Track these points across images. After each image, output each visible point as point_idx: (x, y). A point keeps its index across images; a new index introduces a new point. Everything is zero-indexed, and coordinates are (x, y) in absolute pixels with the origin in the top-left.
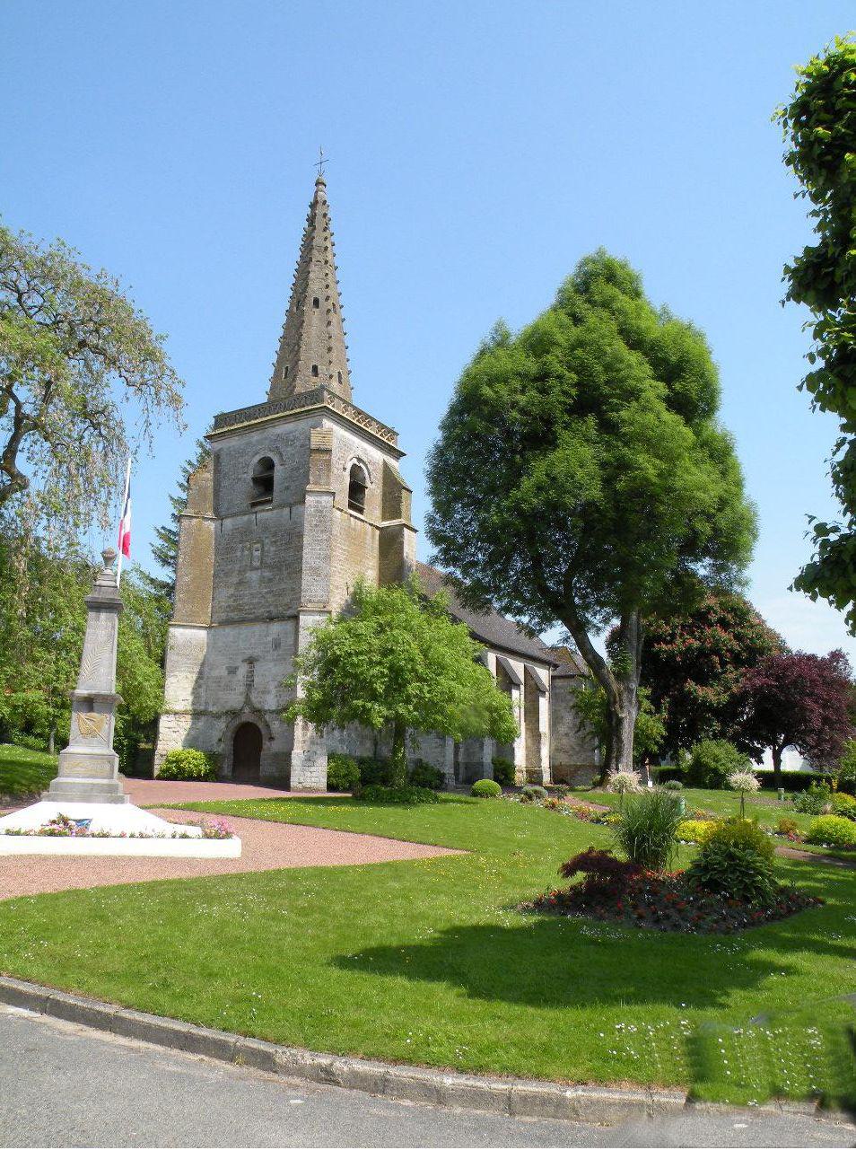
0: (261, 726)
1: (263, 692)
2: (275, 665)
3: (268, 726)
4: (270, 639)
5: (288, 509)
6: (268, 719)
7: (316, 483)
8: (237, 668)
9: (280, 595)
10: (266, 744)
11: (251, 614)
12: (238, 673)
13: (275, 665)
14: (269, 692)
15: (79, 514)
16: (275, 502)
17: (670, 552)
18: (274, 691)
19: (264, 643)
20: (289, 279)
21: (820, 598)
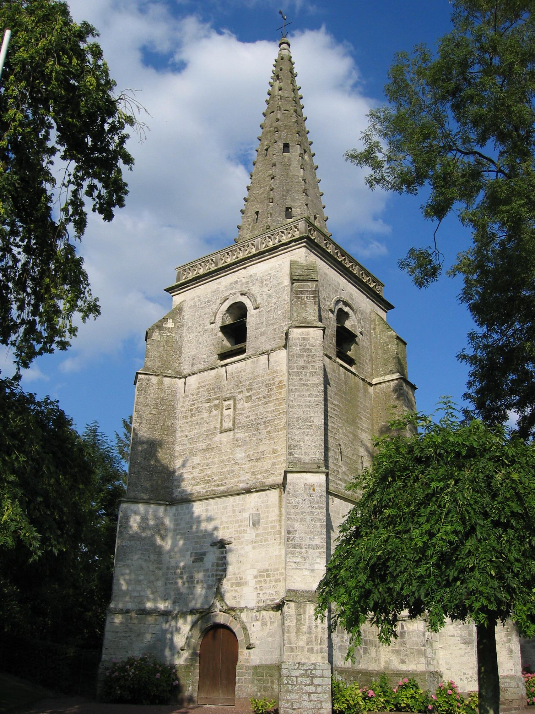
0: (236, 629)
1: (239, 584)
2: (254, 548)
3: (245, 629)
4: (246, 515)
5: (266, 356)
6: (245, 620)
7: (312, 487)
8: (204, 554)
9: (258, 460)
10: (243, 655)
11: (222, 485)
12: (205, 559)
13: (254, 548)
14: (246, 583)
15: (518, 41)
16: (249, 351)
17: (372, 410)
18: (252, 582)
19: (237, 521)
20: (403, 339)
21: (304, 116)
